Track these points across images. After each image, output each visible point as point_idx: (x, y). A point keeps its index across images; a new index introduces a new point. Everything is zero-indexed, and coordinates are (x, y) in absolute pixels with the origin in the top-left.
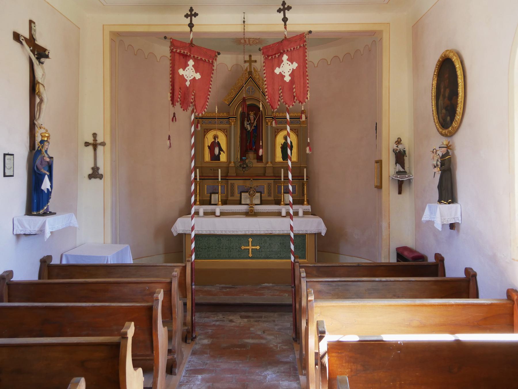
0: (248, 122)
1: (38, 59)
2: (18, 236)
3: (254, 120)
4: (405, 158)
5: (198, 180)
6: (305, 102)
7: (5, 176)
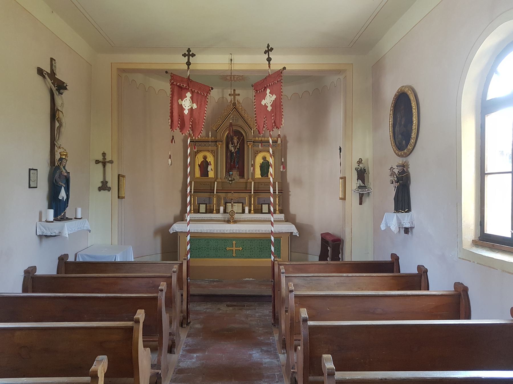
0: (232, 145)
1: (58, 90)
2: (41, 237)
3: (238, 144)
4: (365, 175)
5: (192, 193)
6: (281, 128)
7: (30, 187)
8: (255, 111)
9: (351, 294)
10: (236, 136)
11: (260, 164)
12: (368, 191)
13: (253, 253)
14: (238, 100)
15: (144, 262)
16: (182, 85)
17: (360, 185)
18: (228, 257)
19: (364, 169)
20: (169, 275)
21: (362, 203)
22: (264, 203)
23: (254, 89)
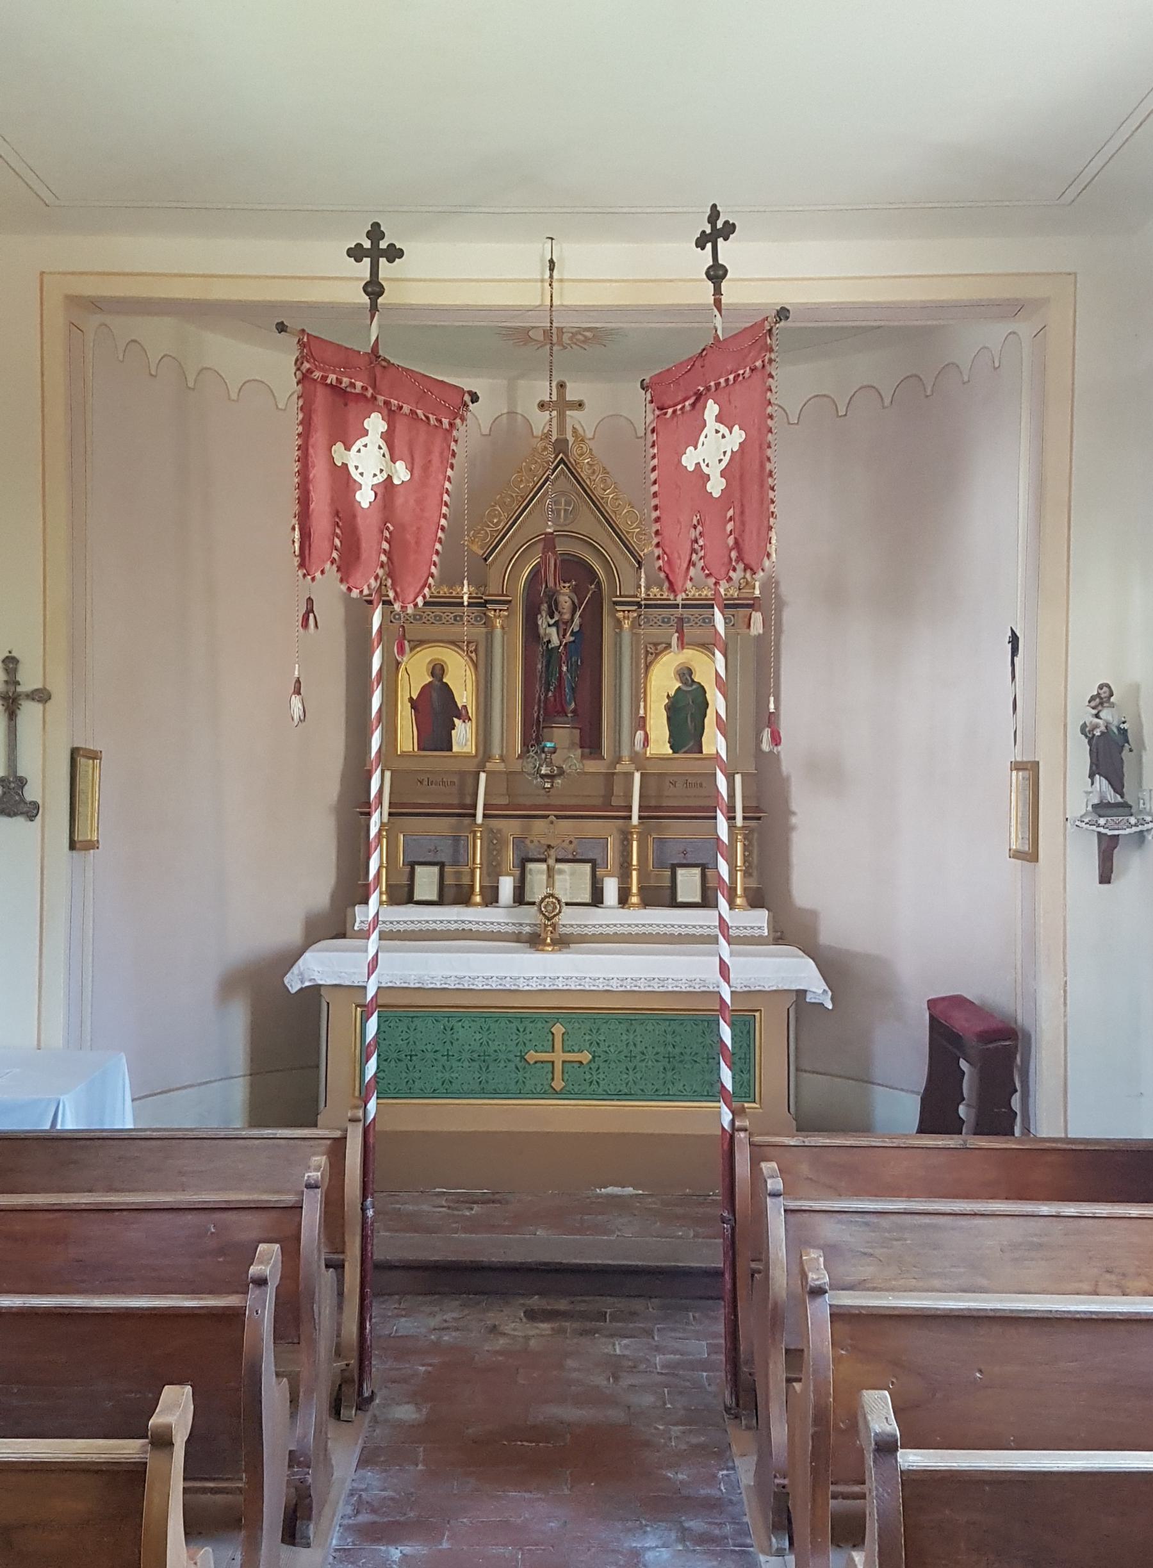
0: (552, 617)
4: (1125, 754)
6: (763, 570)
8: (655, 495)
9: (1078, 1312)
10: (569, 582)
11: (668, 696)
12: (1140, 828)
13: (639, 1075)
14: (577, 426)
15: (180, 1134)
16: (346, 380)
17: (1102, 798)
18: (533, 1094)
19: (1119, 729)
20: (289, 1199)
21: (1113, 876)
22: (685, 862)
23: (652, 402)
